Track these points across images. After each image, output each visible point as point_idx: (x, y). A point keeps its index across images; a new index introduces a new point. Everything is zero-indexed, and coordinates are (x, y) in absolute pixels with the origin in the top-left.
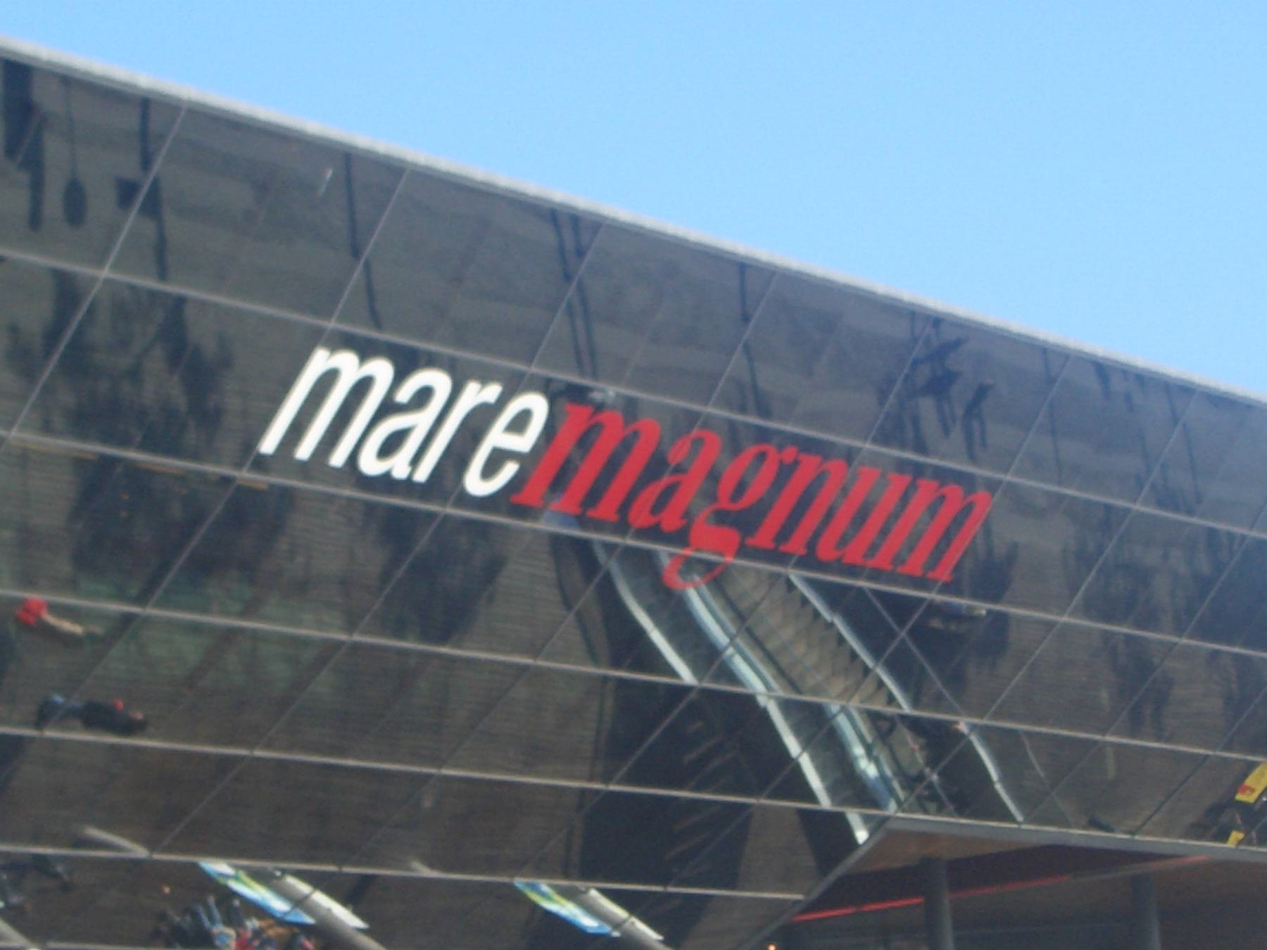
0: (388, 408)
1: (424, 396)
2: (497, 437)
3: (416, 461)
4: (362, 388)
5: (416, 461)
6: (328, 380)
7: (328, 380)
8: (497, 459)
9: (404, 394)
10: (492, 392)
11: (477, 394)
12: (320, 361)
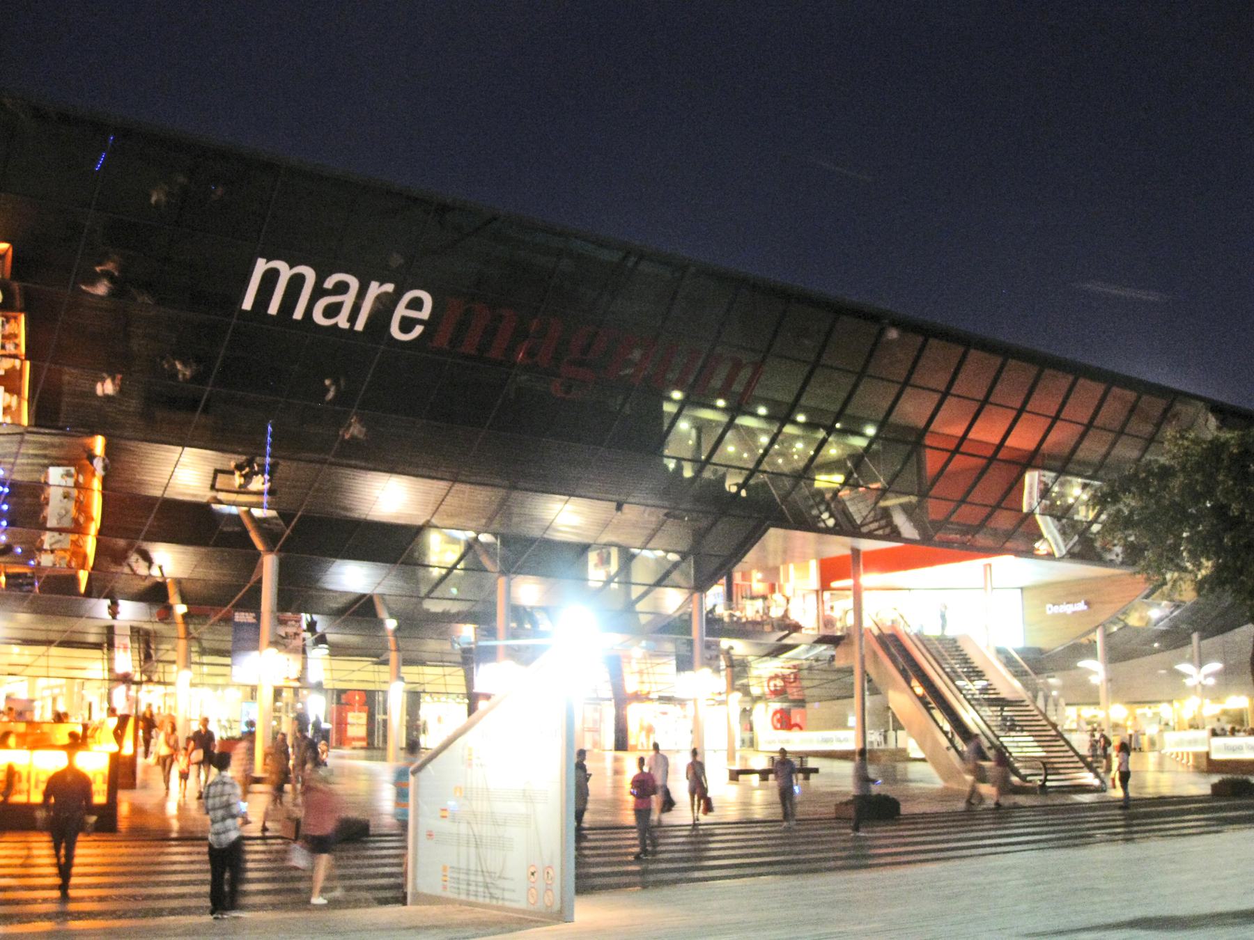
0: (319, 292)
1: (342, 288)
2: (401, 311)
3: (353, 318)
4: (296, 283)
5: (353, 318)
6: (271, 278)
7: (271, 278)
8: (406, 325)
9: (329, 283)
10: (389, 287)
11: (375, 289)
12: (261, 266)
